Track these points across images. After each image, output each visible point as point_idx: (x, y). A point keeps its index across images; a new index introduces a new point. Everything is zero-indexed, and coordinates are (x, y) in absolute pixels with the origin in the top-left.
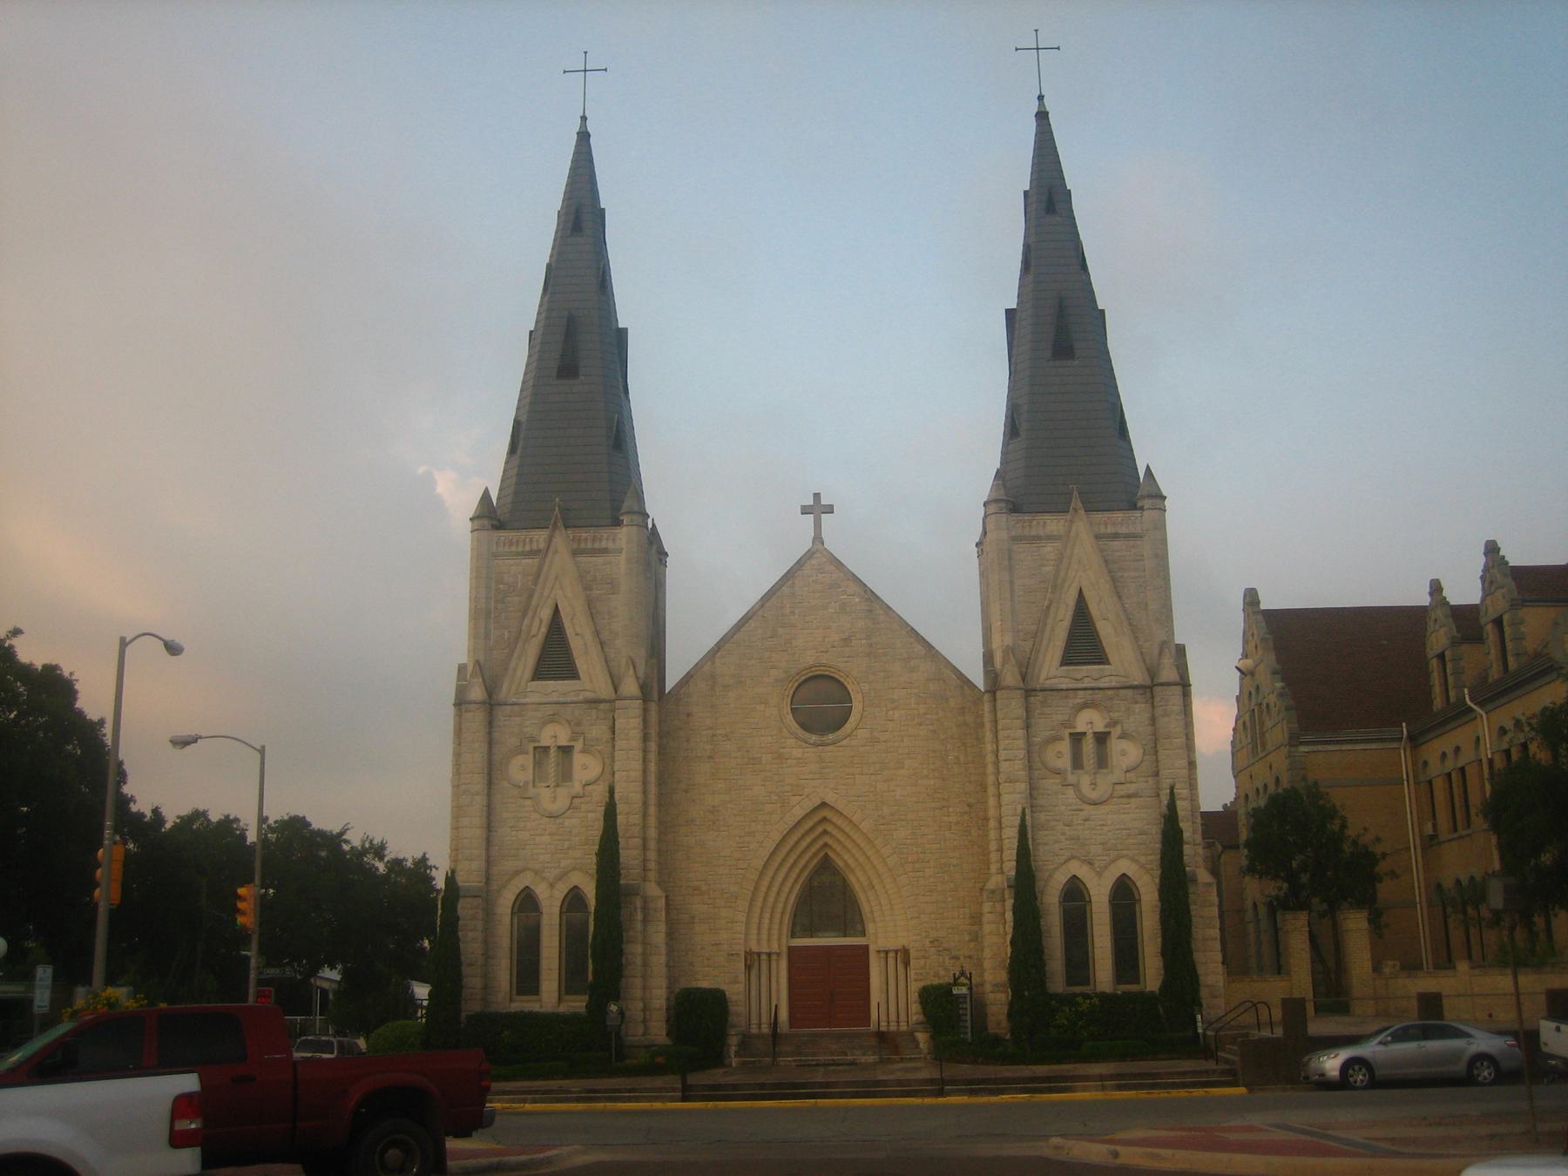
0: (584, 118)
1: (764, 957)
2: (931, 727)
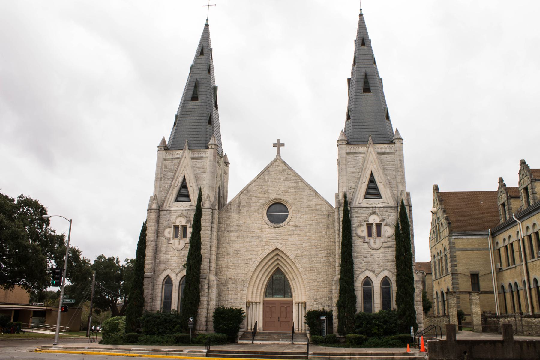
0: (207, 20)
1: (254, 304)
2: (316, 222)
